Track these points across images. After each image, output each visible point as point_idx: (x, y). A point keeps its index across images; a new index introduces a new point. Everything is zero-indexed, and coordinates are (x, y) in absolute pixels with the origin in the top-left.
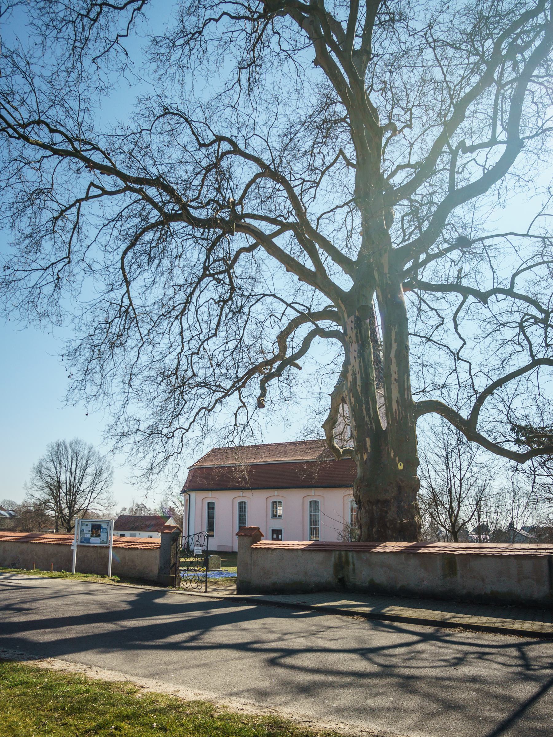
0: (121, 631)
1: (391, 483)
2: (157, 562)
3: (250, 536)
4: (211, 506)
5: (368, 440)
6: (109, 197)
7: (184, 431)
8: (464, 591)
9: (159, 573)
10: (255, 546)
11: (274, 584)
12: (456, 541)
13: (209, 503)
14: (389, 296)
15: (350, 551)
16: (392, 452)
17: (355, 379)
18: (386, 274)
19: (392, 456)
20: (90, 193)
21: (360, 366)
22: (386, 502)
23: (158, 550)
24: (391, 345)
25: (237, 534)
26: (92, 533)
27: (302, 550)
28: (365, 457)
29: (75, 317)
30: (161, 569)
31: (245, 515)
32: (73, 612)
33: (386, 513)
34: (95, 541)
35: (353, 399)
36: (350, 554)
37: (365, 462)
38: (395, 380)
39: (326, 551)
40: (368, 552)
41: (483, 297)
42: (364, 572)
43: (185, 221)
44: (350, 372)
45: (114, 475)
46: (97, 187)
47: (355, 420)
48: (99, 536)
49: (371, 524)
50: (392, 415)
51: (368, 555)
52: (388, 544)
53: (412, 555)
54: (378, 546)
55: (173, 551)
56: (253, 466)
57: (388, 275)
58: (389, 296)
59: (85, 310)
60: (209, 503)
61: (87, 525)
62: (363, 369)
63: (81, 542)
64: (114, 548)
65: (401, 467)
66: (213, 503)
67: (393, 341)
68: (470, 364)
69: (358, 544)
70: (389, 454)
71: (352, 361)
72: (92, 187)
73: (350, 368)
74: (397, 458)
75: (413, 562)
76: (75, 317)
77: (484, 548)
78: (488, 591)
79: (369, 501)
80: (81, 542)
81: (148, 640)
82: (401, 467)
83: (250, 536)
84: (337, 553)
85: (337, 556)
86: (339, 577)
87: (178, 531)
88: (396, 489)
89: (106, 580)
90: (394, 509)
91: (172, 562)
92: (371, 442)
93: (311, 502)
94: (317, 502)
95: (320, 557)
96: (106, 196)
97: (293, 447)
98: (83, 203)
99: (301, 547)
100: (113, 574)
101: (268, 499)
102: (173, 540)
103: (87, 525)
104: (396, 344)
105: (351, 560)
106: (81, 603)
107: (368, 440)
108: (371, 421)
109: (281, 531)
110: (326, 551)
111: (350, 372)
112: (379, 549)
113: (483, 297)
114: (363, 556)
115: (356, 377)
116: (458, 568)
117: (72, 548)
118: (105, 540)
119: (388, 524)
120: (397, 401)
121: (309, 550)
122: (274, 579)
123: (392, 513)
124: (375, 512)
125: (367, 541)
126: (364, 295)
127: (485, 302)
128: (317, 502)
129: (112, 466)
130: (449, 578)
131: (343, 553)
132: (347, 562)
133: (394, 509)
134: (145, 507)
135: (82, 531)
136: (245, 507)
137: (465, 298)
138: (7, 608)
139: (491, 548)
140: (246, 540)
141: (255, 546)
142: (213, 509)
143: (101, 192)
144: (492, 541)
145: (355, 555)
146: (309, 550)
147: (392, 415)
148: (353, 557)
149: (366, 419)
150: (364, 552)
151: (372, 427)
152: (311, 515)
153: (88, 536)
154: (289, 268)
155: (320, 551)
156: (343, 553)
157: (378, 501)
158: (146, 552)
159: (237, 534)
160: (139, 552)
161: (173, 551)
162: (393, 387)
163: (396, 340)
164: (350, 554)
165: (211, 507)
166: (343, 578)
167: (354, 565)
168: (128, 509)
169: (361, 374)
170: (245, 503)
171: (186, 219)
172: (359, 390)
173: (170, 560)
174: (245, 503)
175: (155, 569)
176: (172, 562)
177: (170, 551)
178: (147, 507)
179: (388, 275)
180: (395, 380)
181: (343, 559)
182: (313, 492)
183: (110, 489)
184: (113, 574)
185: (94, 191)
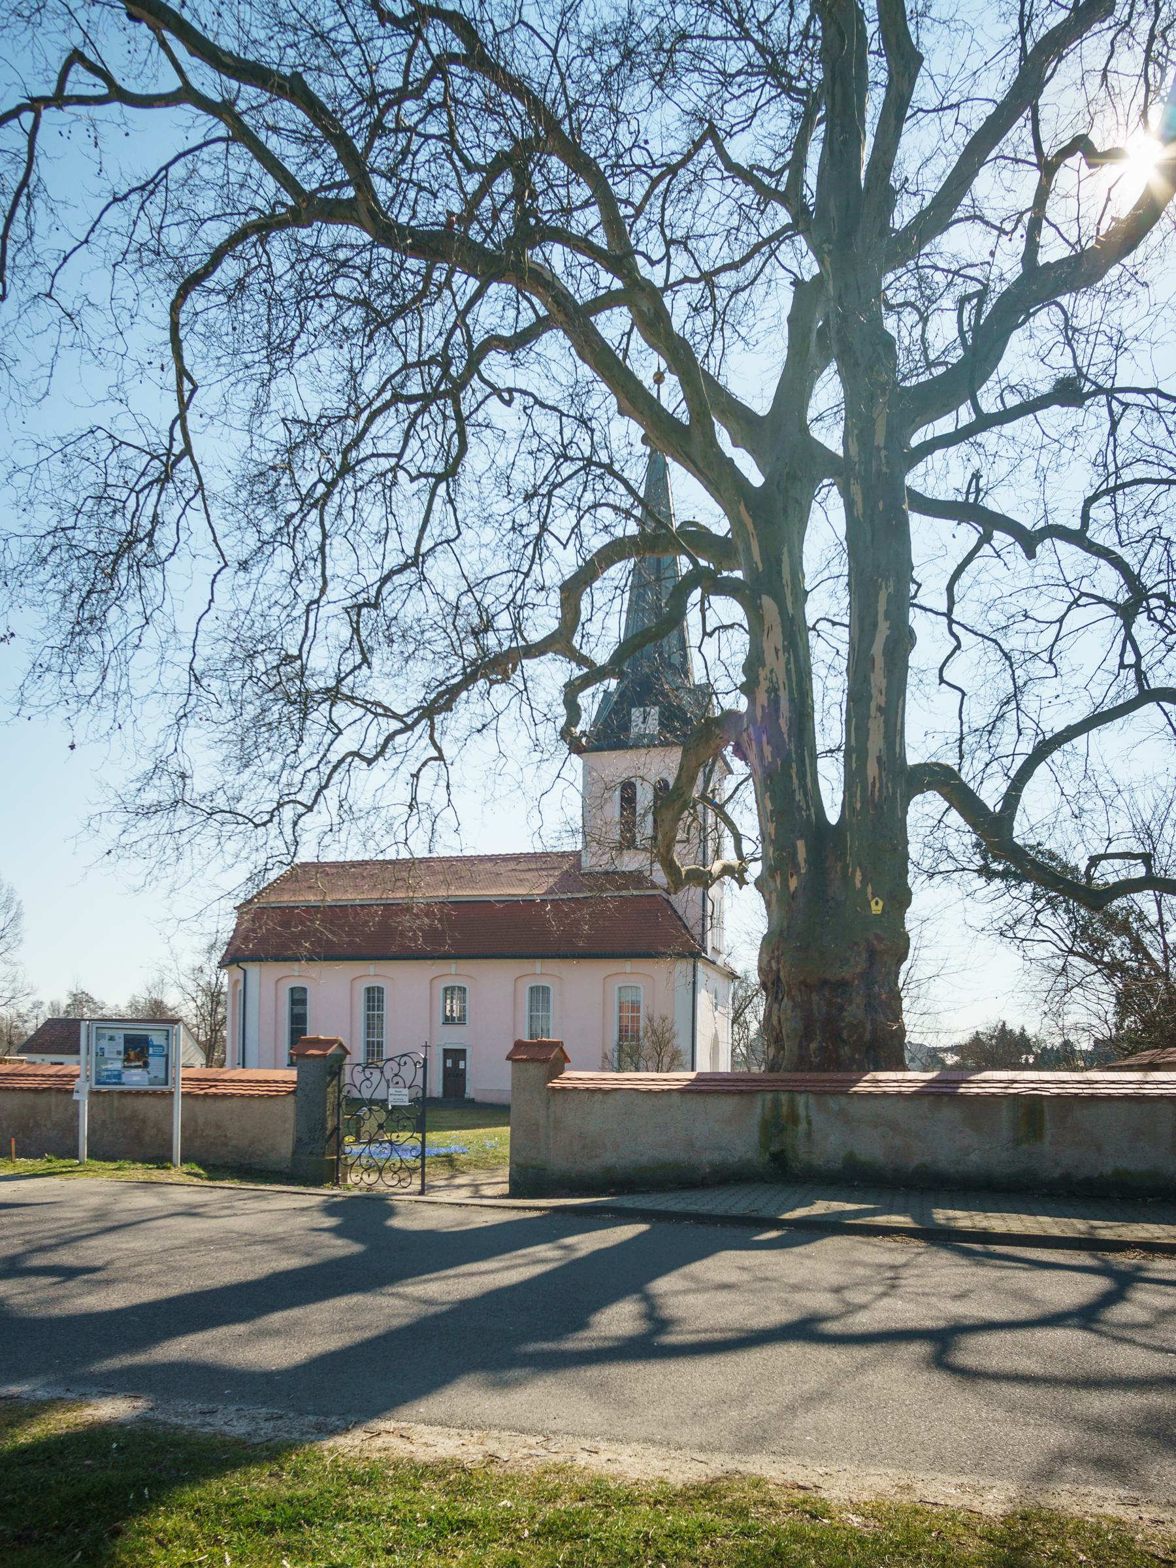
0: (436, 1316)
1: (856, 944)
2: (290, 1126)
3: (546, 1061)
4: (296, 996)
5: (801, 845)
6: (129, 110)
7: (301, 809)
8: (1057, 1173)
9: (294, 1153)
10: (556, 1083)
11: (609, 1170)
12: (637, 1070)
13: (292, 990)
14: (881, 505)
15: (800, 1092)
16: (858, 873)
17: (775, 703)
18: (879, 449)
19: (858, 884)
20: (68, 86)
21: (788, 671)
22: (842, 986)
23: (291, 1099)
24: (875, 625)
25: (508, 1058)
26: (127, 1059)
27: (682, 1092)
28: (793, 883)
29: (17, 469)
30: (299, 1141)
31: (380, 1017)
32: (247, 1267)
33: (841, 1009)
34: (136, 1078)
35: (767, 750)
36: (801, 1100)
37: (794, 896)
38: (879, 709)
39: (741, 1092)
40: (846, 1094)
41: (1028, 541)
42: (832, 1138)
43: (364, 228)
44: (764, 685)
45: (24, 922)
46: (93, 68)
47: (773, 799)
48: (146, 1065)
49: (807, 1035)
50: (864, 789)
51: (843, 1100)
52: (882, 1075)
53: (945, 1099)
54: (859, 1081)
55: (331, 1099)
56: (458, 904)
57: (883, 453)
58: (881, 505)
59: (45, 453)
60: (292, 990)
61: (112, 1038)
62: (794, 678)
63: (98, 1083)
64: (184, 1095)
65: (877, 908)
66: (304, 990)
67: (881, 617)
68: (964, 694)
69: (773, 1076)
70: (847, 880)
71: (769, 657)
72: (78, 67)
73: (762, 673)
74: (869, 889)
75: (949, 1113)
76: (17, 469)
77: (880, 1081)
78: (1108, 1170)
79: (804, 983)
80: (98, 1083)
81: (558, 1336)
82: (877, 908)
83: (546, 1061)
84: (769, 1096)
85: (768, 1104)
86: (773, 1149)
87: (340, 1052)
88: (864, 956)
89: (176, 1173)
90: (858, 1000)
91: (330, 1125)
92: (808, 851)
93: (532, 989)
94: (546, 990)
95: (726, 1105)
96: (116, 106)
97: (489, 866)
98: (49, 115)
99: (675, 1086)
100: (184, 1160)
101: (436, 982)
102: (330, 1074)
103: (112, 1038)
104: (888, 624)
105: (802, 1111)
106: (211, 1242)
107: (801, 845)
108: (807, 802)
109: (464, 1051)
110: (741, 1092)
111: (764, 685)
112: (861, 1088)
113: (1028, 541)
114: (832, 1104)
115: (777, 697)
116: (1048, 1125)
117: (76, 1097)
118: (162, 1075)
119: (845, 1035)
120: (879, 759)
121: (700, 1092)
122: (609, 1158)
123: (854, 1010)
124: (815, 1007)
125: (797, 1070)
126: (797, 501)
127: (1030, 554)
128: (546, 990)
129: (17, 898)
130: (1025, 1146)
131: (784, 1098)
132: (794, 1118)
133: (858, 1000)
134: (90, 1000)
135: (101, 1053)
136: (381, 1000)
137: (986, 539)
138: (12, 1268)
139: (1113, 1082)
140: (533, 1070)
141: (556, 1083)
142: (303, 1002)
143: (102, 90)
144: (1035, 1067)
145: (812, 1100)
146: (700, 1092)
147: (864, 789)
148: (807, 1107)
149: (797, 798)
150: (834, 1094)
151: (809, 816)
152: (531, 1017)
153: (118, 1065)
154: (626, 404)
155: (728, 1092)
156: (784, 1098)
157: (825, 983)
158: (255, 1104)
159: (508, 1058)
160: (235, 1103)
161: (331, 1099)
162: (872, 725)
163: (886, 612)
164: (801, 1100)
165: (298, 998)
166: (783, 1152)
167: (809, 1123)
168: (47, 1004)
169: (791, 692)
170: (380, 990)
171: (365, 218)
172: (784, 728)
173: (325, 1120)
174: (380, 990)
175: (285, 1145)
176: (330, 1125)
177: (325, 1099)
178: (97, 999)
179: (883, 453)
180: (879, 709)
181: (784, 1110)
182: (538, 966)
183: (16, 956)
184: (184, 1160)
185: (81, 82)
